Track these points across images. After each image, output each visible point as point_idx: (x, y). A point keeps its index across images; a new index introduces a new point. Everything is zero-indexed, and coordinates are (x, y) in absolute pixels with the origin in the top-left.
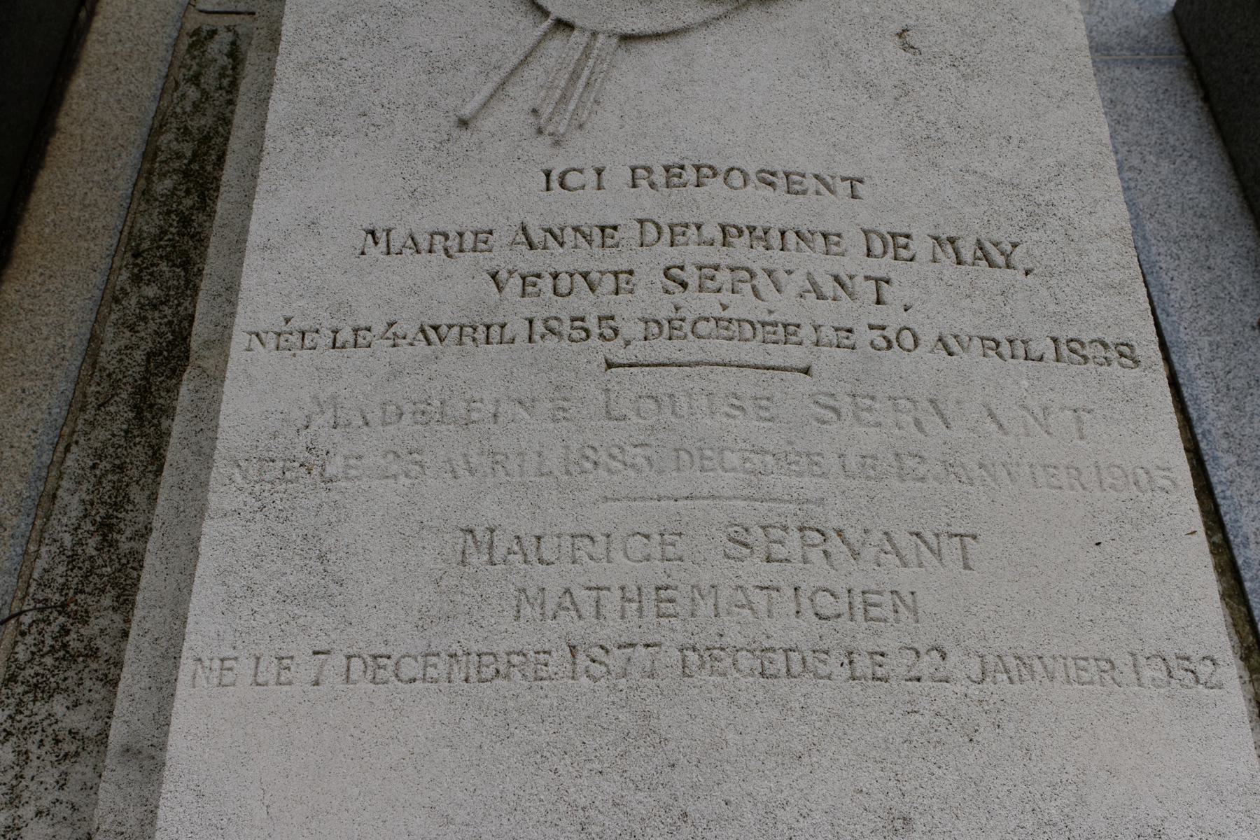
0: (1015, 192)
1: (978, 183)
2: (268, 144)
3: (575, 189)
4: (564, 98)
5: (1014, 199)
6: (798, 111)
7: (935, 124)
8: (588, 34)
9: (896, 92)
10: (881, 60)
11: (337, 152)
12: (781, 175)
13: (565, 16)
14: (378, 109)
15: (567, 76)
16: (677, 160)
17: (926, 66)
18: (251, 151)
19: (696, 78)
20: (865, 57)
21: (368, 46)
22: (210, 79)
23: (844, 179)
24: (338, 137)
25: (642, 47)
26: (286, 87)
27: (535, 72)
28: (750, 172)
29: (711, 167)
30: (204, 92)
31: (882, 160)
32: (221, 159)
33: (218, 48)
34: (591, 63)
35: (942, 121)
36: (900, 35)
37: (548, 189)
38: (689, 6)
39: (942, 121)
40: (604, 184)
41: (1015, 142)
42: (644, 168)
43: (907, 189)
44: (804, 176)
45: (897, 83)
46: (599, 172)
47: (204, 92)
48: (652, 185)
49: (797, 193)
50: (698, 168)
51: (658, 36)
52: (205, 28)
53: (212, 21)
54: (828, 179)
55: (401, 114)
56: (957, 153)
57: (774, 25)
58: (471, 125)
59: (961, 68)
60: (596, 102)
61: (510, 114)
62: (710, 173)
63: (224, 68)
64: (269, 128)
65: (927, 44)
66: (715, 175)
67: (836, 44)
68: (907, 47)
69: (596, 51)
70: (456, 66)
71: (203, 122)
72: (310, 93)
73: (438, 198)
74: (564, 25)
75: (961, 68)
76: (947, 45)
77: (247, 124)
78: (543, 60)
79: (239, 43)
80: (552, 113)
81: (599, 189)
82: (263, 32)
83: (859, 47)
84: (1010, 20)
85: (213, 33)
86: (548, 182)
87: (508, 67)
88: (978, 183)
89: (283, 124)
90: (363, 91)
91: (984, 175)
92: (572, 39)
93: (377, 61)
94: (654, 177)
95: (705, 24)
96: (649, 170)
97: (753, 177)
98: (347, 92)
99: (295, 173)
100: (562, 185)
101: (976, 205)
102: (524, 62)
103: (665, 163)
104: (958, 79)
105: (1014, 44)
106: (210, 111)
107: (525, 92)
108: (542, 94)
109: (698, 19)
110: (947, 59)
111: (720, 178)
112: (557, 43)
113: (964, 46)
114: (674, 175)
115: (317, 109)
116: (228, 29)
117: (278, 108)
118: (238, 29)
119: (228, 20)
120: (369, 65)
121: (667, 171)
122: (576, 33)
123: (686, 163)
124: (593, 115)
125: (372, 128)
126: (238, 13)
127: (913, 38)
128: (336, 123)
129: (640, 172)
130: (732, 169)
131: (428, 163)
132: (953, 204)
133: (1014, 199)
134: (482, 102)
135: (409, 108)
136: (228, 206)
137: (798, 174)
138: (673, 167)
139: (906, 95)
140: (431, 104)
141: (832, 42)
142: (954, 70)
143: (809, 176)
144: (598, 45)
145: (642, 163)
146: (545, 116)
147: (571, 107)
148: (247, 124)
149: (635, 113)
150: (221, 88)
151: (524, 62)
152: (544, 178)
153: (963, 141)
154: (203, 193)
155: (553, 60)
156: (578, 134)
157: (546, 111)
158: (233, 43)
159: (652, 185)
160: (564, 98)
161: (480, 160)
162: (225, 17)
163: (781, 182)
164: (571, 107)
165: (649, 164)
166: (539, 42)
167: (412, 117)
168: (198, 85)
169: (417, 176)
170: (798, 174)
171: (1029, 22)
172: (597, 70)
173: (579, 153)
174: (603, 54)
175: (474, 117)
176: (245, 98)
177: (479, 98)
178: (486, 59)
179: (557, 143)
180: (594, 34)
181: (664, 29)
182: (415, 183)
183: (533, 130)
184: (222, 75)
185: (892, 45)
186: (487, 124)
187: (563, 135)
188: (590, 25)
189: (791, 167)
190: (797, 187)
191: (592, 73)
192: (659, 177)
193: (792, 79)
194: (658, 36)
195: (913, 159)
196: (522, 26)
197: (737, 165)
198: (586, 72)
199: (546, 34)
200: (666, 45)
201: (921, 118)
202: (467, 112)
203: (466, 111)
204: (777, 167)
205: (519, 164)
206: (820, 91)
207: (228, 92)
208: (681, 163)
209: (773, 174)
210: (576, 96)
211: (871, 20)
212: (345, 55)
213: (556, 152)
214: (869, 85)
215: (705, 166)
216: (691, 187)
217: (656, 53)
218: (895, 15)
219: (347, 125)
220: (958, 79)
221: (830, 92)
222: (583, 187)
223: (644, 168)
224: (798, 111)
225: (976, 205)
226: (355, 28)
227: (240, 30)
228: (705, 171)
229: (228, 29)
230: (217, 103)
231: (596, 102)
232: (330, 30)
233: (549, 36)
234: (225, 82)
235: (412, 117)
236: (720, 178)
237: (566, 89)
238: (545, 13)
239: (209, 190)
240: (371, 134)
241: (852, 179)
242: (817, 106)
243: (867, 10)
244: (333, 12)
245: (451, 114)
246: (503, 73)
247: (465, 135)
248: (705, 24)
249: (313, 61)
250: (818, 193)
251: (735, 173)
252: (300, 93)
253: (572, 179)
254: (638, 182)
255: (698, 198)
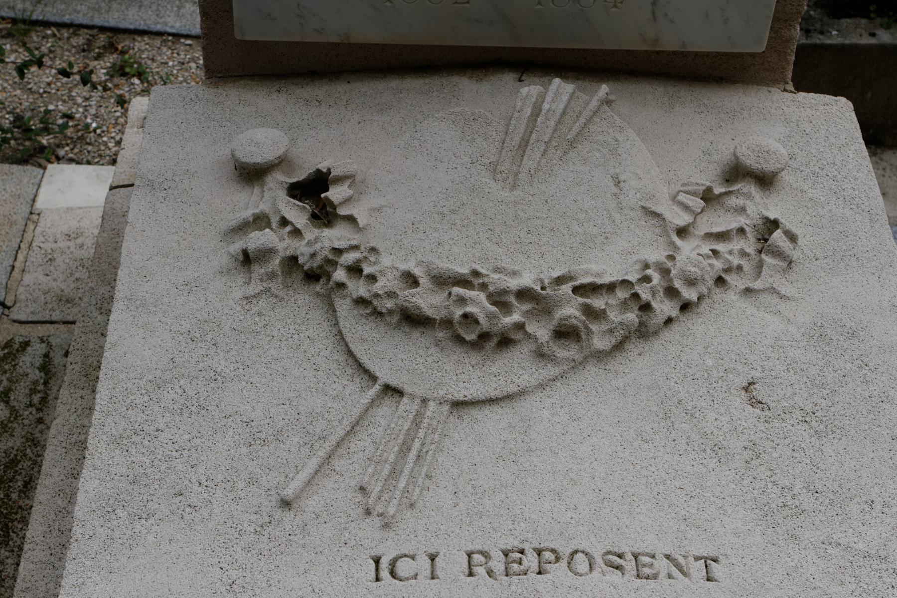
0: (884, 566)
1: (843, 557)
2: (77, 530)
3: (407, 579)
4: (394, 473)
5: (883, 574)
6: (644, 480)
7: (791, 489)
8: (417, 401)
9: (747, 454)
10: (727, 418)
11: (150, 538)
12: (629, 557)
13: (394, 382)
14: (196, 487)
15: (396, 449)
16: (516, 543)
17: (776, 423)
18: (59, 502)
19: (533, 447)
20: (711, 416)
21: (186, 415)
22: (19, 396)
23: (697, 559)
24: (151, 521)
25: (475, 412)
26: (98, 463)
27: (362, 443)
28: (595, 555)
29: (553, 551)
30: (13, 410)
31: (736, 534)
32: (29, 485)
33: (29, 361)
34: (421, 434)
35: (798, 486)
36: (746, 389)
37: (378, 579)
38: (523, 368)
39: (798, 486)
40: (438, 572)
41: (878, 507)
42: (481, 553)
43: (766, 568)
44: (653, 557)
45: (747, 444)
46: (433, 558)
47: (13, 410)
48: (490, 573)
49: (647, 578)
50: (539, 552)
51: (491, 401)
52: (18, 339)
53: (25, 331)
54: (681, 560)
55: (219, 493)
56: (817, 523)
57: (613, 383)
58: (295, 505)
59: (814, 424)
60: (429, 477)
61: (338, 492)
62: (552, 557)
63: (35, 383)
64: (79, 511)
65: (775, 398)
66: (558, 559)
67: (679, 402)
68: (756, 402)
69: (426, 421)
70: (278, 436)
71: (10, 444)
72: (124, 470)
73: (258, 591)
74: (392, 391)
75: (814, 424)
76: (796, 399)
77: (55, 472)
78: (371, 430)
79: (52, 355)
80: (381, 491)
81: (433, 578)
82: (77, 368)
83: (704, 404)
84: (860, 367)
85: (26, 344)
86: (377, 570)
87: (333, 439)
88: (843, 557)
89: (94, 506)
90: (179, 467)
91: (848, 547)
92: (402, 407)
93: (195, 433)
94: (493, 564)
95: (541, 386)
96: (486, 554)
97: (599, 561)
98: (163, 468)
99: (104, 564)
100: (393, 574)
101: (842, 583)
102: (351, 432)
103: (504, 547)
104: (811, 436)
105: (867, 394)
106: (18, 432)
107: (352, 467)
108: (370, 470)
109: (534, 382)
110: (798, 414)
111: (563, 563)
112: (386, 408)
113: (815, 399)
114: (514, 561)
115: (130, 488)
116: (42, 340)
117: (89, 487)
118: (51, 339)
119: (41, 330)
120: (187, 437)
121: (506, 555)
122: (405, 400)
123: (526, 546)
124: (425, 492)
125: (189, 510)
126: (52, 322)
127: (760, 391)
128: (150, 504)
129: (477, 558)
130: (576, 552)
131: (247, 549)
132: (818, 584)
133: (883, 574)
134: (306, 480)
135: (228, 486)
136: (32, 566)
137: (647, 555)
138: (512, 551)
139: (758, 457)
140: (252, 481)
141: (675, 399)
142: (806, 426)
143: (660, 556)
144: (429, 413)
145: (479, 547)
146: (374, 495)
147: (402, 485)
148: (55, 472)
149: (469, 488)
150: (31, 405)
151: (351, 432)
152: (373, 565)
153: (823, 508)
154: (6, 525)
155: (381, 429)
156: (408, 513)
157: (375, 489)
158: (46, 355)
159: (490, 573)
160: (394, 473)
161: (304, 546)
162: (40, 327)
163: (629, 564)
164: (402, 485)
165: (486, 548)
166: (367, 410)
167: (231, 496)
168: (7, 402)
169: (235, 566)
170: (647, 555)
171: (881, 369)
172: (428, 440)
173: (409, 537)
174: (435, 423)
175: (298, 497)
176: (55, 441)
177: (303, 476)
178: (310, 428)
179: (386, 526)
180: (424, 401)
181: (498, 394)
182: (233, 574)
183: (361, 510)
184: (33, 391)
185: (739, 400)
186: (312, 503)
187: (392, 517)
188: (420, 391)
189: (640, 548)
190: (647, 571)
191: (423, 444)
192: (497, 563)
193: (636, 444)
194: (491, 401)
195: (770, 531)
196: (348, 391)
197: (581, 548)
198: (417, 445)
199: (373, 401)
200: (500, 411)
201: (775, 483)
202: (290, 492)
203: (289, 492)
204: (625, 549)
205: (346, 550)
206: (666, 457)
207: (39, 410)
208: (521, 546)
209: (620, 556)
210: (406, 472)
211: (715, 372)
212: (162, 426)
213: (386, 535)
214: (717, 447)
215: (547, 550)
216: (532, 575)
217: (491, 420)
218: (740, 367)
219: (162, 506)
220: (811, 436)
221: (676, 457)
222: (415, 577)
223: (481, 553)
224: (644, 480)
225: (842, 583)
226: (173, 395)
227: (54, 341)
228: (548, 555)
229: (42, 340)
230: (26, 422)
231: (429, 477)
232: (146, 398)
233: (377, 403)
234: (36, 398)
235: (231, 496)
236: (563, 563)
237: (396, 462)
238: (373, 378)
239: (13, 521)
240: (187, 517)
241: (706, 559)
242: (664, 474)
243: (710, 362)
244: (150, 377)
245: (273, 492)
246: (328, 446)
247: (288, 516)
248: (541, 386)
249: (128, 433)
250: (670, 576)
251: (580, 557)
252: (113, 470)
253: (403, 568)
254: (475, 569)
255: (540, 589)
